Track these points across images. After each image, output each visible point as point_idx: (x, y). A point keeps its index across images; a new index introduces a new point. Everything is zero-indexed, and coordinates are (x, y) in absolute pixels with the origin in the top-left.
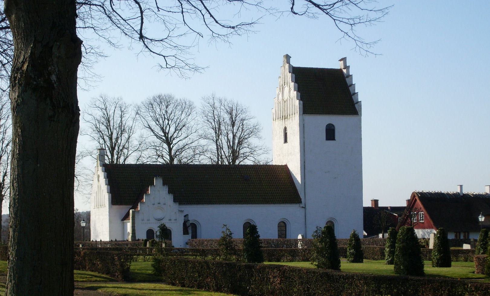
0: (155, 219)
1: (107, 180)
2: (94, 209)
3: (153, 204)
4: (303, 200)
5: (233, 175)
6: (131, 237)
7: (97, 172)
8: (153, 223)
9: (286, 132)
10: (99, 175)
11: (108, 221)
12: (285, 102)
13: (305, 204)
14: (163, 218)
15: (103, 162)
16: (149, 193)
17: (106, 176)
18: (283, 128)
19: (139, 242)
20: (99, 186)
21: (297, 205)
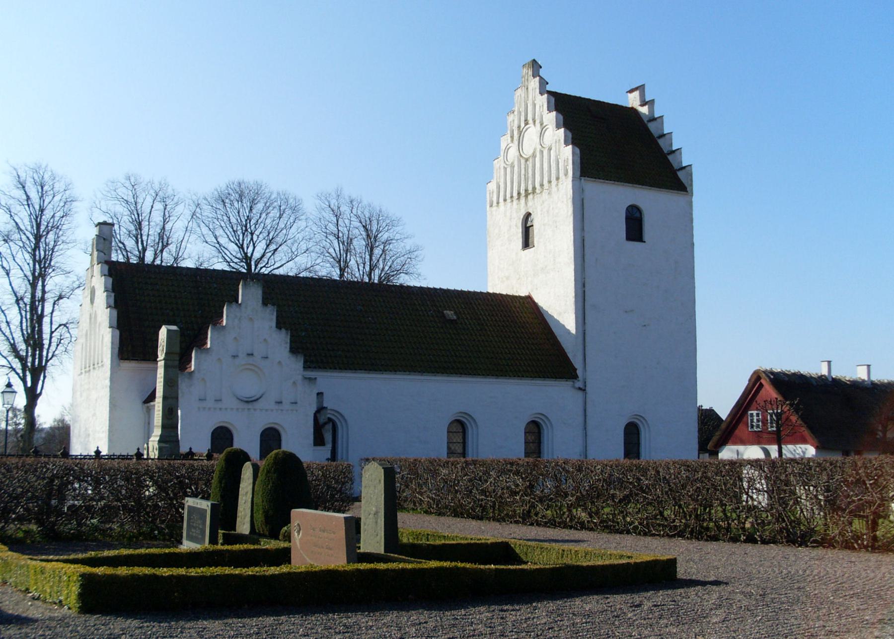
0: (235, 395)
1: (111, 296)
2: (79, 375)
3: (234, 357)
4: (579, 372)
5: (420, 309)
6: (159, 441)
7: (91, 281)
8: (232, 409)
9: (529, 224)
10: (93, 287)
11: (108, 402)
12: (527, 160)
13: (585, 383)
14: (260, 397)
15: (105, 254)
16: (224, 324)
17: (110, 286)
18: (519, 219)
19: (196, 463)
20: (93, 316)
21: (570, 383)
